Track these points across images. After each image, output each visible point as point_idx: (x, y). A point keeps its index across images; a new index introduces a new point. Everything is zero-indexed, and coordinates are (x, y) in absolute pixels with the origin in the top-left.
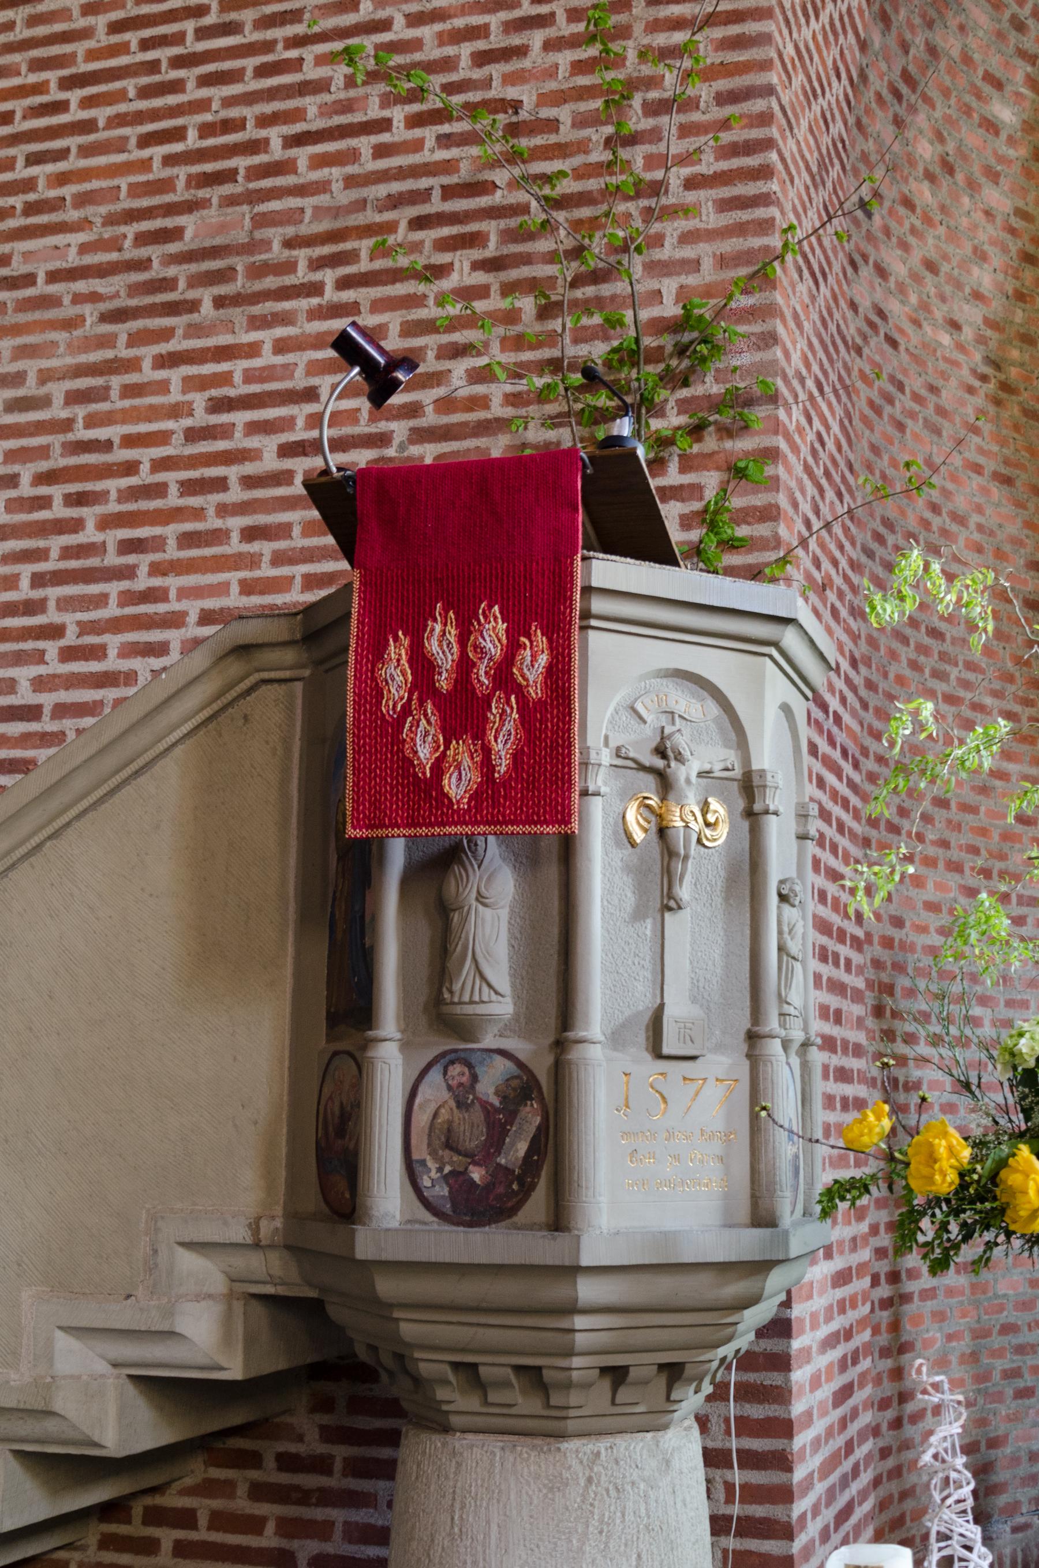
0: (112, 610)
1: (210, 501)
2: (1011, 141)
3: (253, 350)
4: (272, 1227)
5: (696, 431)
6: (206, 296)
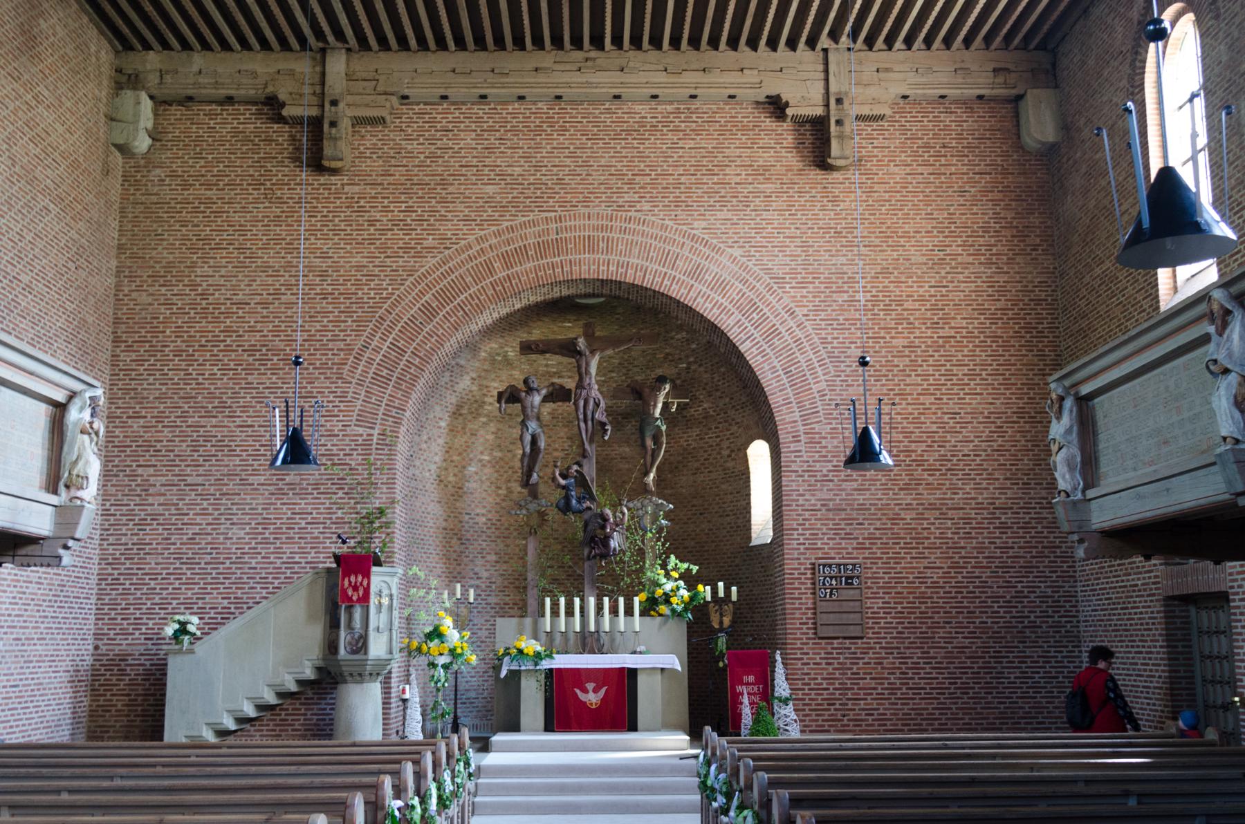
0: (272, 550)
1: (292, 531)
3: (300, 504)
4: (320, 656)
5: (381, 527)
6: (291, 492)
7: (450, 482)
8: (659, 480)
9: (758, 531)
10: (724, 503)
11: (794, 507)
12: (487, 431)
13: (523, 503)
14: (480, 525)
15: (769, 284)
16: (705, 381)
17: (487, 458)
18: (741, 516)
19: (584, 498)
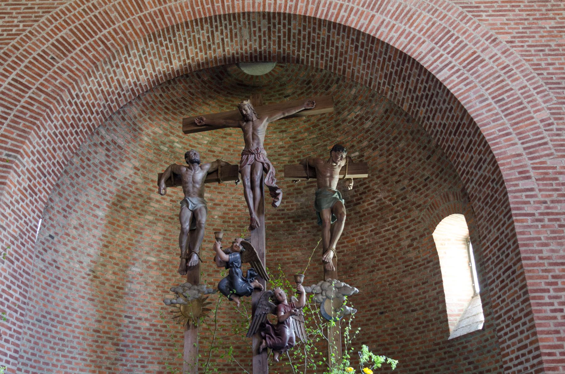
2: (101, 219)
7: (107, 280)
8: (339, 262)
9: (456, 323)
10: (408, 297)
11: (537, 261)
12: (154, 231)
13: (181, 291)
14: (142, 330)
15: (462, 13)
16: (379, 167)
17: (154, 260)
18: (431, 309)
19: (252, 276)
